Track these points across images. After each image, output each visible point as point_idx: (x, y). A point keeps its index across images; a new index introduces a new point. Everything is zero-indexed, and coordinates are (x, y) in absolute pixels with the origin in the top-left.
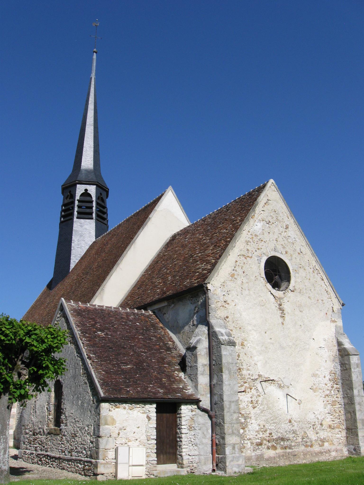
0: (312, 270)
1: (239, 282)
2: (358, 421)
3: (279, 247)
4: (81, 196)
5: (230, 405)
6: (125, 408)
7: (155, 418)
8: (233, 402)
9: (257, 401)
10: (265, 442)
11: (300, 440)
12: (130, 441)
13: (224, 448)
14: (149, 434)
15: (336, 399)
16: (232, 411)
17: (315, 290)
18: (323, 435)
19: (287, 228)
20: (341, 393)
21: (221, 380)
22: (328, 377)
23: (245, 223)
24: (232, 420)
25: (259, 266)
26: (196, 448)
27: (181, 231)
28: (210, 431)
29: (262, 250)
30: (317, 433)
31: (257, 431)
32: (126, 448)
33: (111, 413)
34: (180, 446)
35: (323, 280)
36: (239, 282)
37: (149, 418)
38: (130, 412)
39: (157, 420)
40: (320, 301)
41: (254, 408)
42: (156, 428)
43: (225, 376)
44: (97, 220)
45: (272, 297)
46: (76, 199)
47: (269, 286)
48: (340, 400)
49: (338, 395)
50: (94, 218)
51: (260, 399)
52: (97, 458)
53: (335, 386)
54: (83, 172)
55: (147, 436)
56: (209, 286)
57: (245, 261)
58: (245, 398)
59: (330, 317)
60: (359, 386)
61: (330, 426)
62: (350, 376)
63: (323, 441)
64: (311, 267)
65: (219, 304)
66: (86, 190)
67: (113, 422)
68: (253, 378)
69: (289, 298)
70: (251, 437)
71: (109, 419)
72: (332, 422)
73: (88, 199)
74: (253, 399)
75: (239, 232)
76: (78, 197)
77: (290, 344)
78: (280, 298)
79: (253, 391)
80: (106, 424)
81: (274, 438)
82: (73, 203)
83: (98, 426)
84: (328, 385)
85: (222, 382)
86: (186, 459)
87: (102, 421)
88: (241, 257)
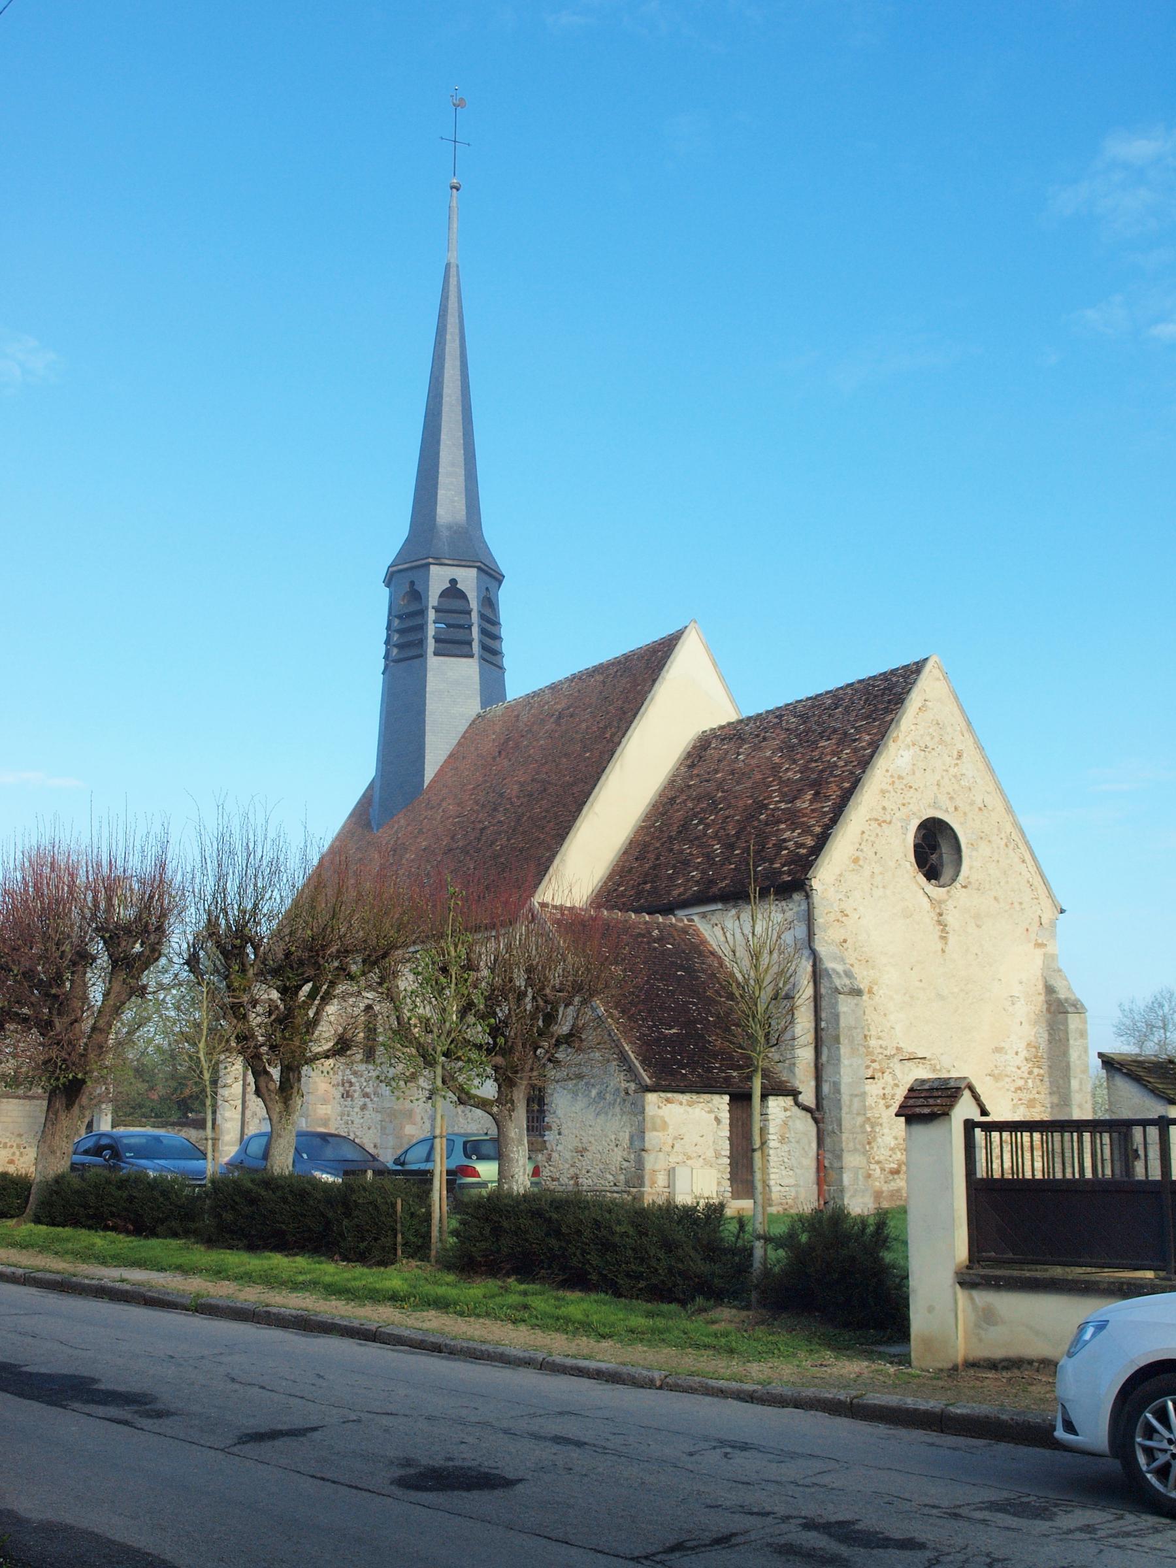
0: (1003, 843)
1: (866, 872)
3: (944, 800)
4: (441, 596)
5: (851, 1101)
6: (681, 1104)
8: (856, 1096)
9: (893, 1095)
12: (689, 1158)
13: (841, 1174)
15: (1037, 1096)
17: (1007, 882)
19: (960, 756)
21: (836, 1060)
22: (1024, 1054)
23: (880, 754)
25: (904, 840)
27: (722, 728)
28: (814, 1145)
29: (911, 806)
31: (892, 1149)
32: (687, 1171)
33: (660, 1112)
35: (1023, 861)
36: (866, 872)
39: (731, 1125)
40: (1016, 905)
42: (730, 1139)
43: (844, 1050)
45: (926, 899)
46: (430, 606)
47: (921, 879)
50: (476, 656)
52: (642, 1185)
53: (1036, 1071)
54: (445, 533)
55: (715, 1151)
56: (815, 884)
57: (878, 830)
59: (1033, 936)
62: (1065, 1053)
64: (1003, 835)
66: (453, 582)
67: (665, 1125)
68: (888, 1053)
69: (957, 899)
70: (882, 1158)
71: (659, 1121)
73: (457, 604)
74: (886, 1092)
75: (868, 771)
76: (433, 600)
77: (956, 990)
78: (940, 902)
79: (887, 1077)
82: (422, 613)
84: (1023, 1069)
85: (839, 1060)
86: (776, 1192)
87: (648, 1125)
88: (872, 823)
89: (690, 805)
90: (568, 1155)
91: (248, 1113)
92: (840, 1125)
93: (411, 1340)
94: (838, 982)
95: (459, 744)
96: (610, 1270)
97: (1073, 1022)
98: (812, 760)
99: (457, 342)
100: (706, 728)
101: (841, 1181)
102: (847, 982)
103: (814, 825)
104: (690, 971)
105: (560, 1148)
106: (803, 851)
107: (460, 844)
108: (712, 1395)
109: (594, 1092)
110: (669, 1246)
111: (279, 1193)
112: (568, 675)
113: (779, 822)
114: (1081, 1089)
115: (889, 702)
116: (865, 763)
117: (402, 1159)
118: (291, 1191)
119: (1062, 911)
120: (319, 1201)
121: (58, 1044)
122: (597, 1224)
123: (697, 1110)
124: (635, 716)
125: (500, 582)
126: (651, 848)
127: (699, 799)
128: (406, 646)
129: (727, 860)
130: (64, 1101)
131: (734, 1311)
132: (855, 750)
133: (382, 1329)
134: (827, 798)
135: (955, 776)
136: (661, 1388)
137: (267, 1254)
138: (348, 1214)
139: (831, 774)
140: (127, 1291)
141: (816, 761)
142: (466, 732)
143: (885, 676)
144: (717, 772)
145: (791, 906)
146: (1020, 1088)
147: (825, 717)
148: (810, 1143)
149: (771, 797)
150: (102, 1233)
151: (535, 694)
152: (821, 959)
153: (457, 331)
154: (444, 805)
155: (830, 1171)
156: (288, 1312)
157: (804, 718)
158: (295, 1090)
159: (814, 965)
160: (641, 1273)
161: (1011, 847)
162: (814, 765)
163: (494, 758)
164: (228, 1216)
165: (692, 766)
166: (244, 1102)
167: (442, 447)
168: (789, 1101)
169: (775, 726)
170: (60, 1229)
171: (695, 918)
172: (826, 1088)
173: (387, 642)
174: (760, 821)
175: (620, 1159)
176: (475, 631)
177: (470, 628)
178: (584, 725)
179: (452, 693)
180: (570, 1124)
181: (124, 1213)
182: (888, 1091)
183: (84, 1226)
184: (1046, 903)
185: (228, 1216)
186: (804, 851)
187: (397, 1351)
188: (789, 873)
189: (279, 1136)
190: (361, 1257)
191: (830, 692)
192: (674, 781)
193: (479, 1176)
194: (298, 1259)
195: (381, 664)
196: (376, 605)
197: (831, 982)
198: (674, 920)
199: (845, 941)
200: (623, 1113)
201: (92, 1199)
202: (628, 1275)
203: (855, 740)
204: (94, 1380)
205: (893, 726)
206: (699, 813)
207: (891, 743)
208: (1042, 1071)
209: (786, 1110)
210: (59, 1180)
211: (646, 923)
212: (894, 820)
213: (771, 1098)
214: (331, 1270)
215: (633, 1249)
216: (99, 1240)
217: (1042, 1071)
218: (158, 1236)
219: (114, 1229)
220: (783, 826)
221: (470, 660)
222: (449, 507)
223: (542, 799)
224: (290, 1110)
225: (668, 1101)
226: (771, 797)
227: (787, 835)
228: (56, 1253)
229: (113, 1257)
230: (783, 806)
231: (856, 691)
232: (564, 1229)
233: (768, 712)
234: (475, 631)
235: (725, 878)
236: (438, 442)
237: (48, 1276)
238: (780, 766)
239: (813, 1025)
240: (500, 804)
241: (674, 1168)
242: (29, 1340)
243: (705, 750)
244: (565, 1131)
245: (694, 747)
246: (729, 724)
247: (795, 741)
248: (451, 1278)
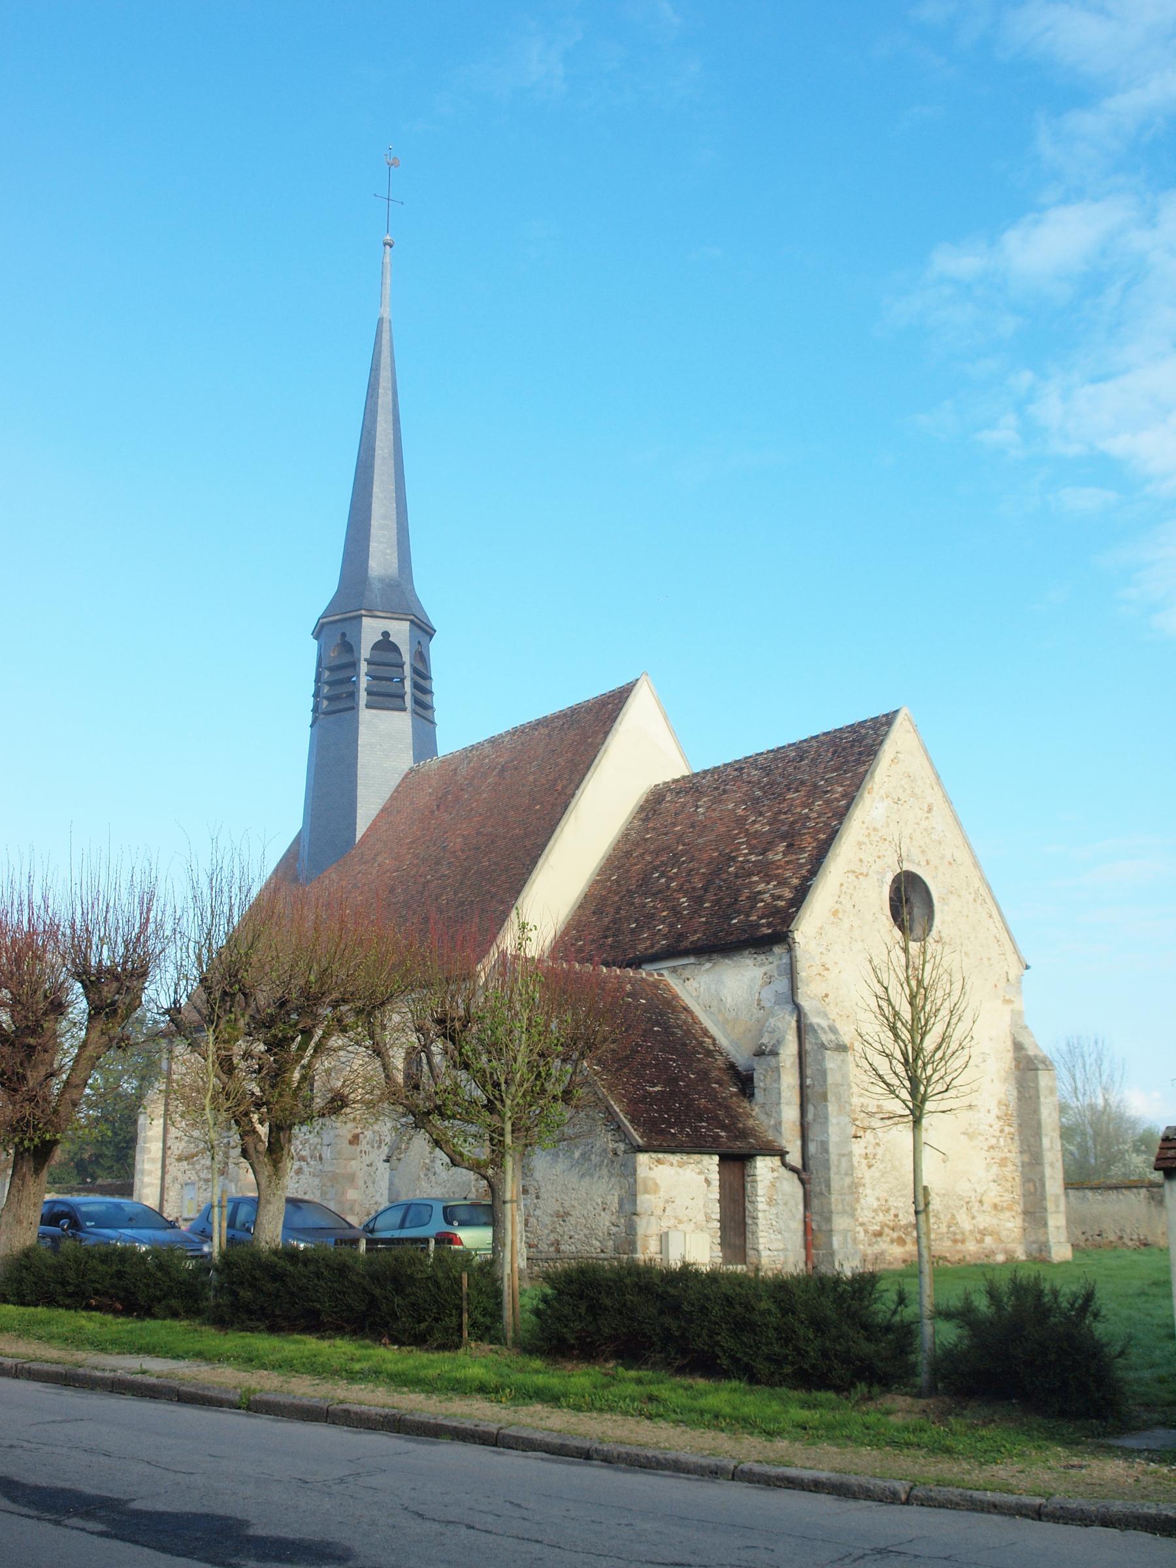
2: (1048, 1197)
6: (672, 1165)
7: (718, 1183)
8: (844, 1155)
9: (875, 1155)
10: (887, 1230)
11: (944, 1229)
12: (680, 1222)
14: (709, 1211)
15: (1008, 1155)
16: (843, 1172)
17: (976, 938)
18: (984, 1221)
19: (930, 810)
20: (1017, 1143)
22: (995, 1111)
23: (857, 805)
24: (842, 1188)
26: (779, 1236)
27: (676, 781)
28: (801, 1207)
30: (973, 1218)
31: (875, 1211)
34: (753, 1233)
37: (708, 1181)
38: (679, 1169)
40: (985, 961)
41: (870, 1167)
42: (719, 1201)
43: (832, 1108)
44: (415, 712)
48: (1014, 1156)
49: (1011, 1147)
51: (880, 1151)
52: (634, 1251)
53: (1007, 1129)
54: (377, 585)
55: (706, 1214)
56: (798, 936)
58: (857, 1148)
60: (1054, 1130)
61: (995, 1206)
63: (983, 1233)
65: (814, 971)
66: (386, 634)
70: (865, 1220)
71: (650, 1183)
72: (999, 1199)
73: (390, 657)
76: (365, 652)
80: (646, 1192)
81: (902, 1223)
82: (354, 665)
83: (632, 1196)
84: (995, 1127)
85: (826, 1118)
87: (640, 1187)
88: (850, 875)
89: (648, 858)
90: (547, 1220)
91: (168, 1178)
92: (828, 1186)
93: (548, 1444)
94: (825, 1038)
95: (392, 798)
96: (745, 1353)
97: (1044, 1080)
98: (780, 812)
99: (390, 397)
100: (659, 781)
101: (831, 1245)
102: (833, 1038)
103: (791, 877)
104: (667, 1028)
105: (538, 1212)
106: (782, 903)
107: (401, 898)
108: (982, 1511)
109: (577, 1154)
110: (819, 1325)
111: (312, 1268)
112: (509, 728)
113: (750, 875)
114: (1052, 1148)
115: (860, 753)
116: (842, 815)
117: (371, 1226)
118: (327, 1266)
119: (1027, 967)
120: (363, 1277)
121: (30, 1100)
122: (729, 1301)
123: (688, 1171)
124: (588, 768)
125: (431, 636)
126: (609, 902)
127: (657, 853)
128: (335, 701)
129: (695, 913)
130: (32, 1164)
131: (909, 1400)
132: (828, 802)
133: (507, 1431)
134: (803, 850)
135: (925, 830)
136: (907, 1502)
137: (297, 1337)
138: (399, 1291)
139: (804, 826)
140: (154, 1386)
141: (785, 813)
142: (399, 786)
143: (852, 729)
144: (674, 825)
145: (770, 959)
146: (992, 1147)
147: (791, 770)
148: (797, 1205)
149: (739, 850)
150: (84, 1313)
151: (473, 748)
152: (805, 1014)
153: (390, 385)
154: (380, 859)
155: (819, 1235)
156: (373, 1410)
157: (767, 770)
158: (285, 1152)
159: (798, 1021)
160: (786, 1357)
161: (979, 901)
162: (783, 817)
163: (432, 812)
164: (246, 1294)
165: (646, 820)
166: (164, 1166)
167: (374, 500)
168: (776, 1161)
169: (735, 779)
170: (32, 1309)
171: (665, 972)
172: (812, 1148)
173: (316, 695)
174: (729, 874)
175: (607, 1224)
176: (408, 684)
177: (403, 682)
178: (531, 778)
179: (384, 746)
180: (549, 1187)
181: (113, 1291)
182: (870, 1150)
183: (60, 1306)
184: (1012, 958)
185: (246, 1294)
186: (783, 903)
187: (527, 1457)
188: (769, 925)
189: (268, 1202)
190: (419, 1340)
191: (794, 744)
192: (627, 835)
193: (461, 1243)
194: (338, 1342)
195: (309, 717)
196: (302, 660)
197: (817, 1038)
198: (644, 975)
199: (827, 996)
200: (611, 1175)
201: (71, 1275)
202: (768, 1358)
203: (828, 792)
204: (245, 1524)
205: (868, 777)
206: (659, 866)
207: (866, 795)
208: (1012, 1130)
209: (773, 1170)
210: (27, 1254)
211: (617, 977)
212: (871, 873)
213: (759, 1158)
214: (387, 1355)
215: (776, 1329)
216: (89, 1322)
217: (1012, 1130)
218: (154, 1316)
219: (97, 1308)
220: (755, 878)
221: (403, 713)
222: (381, 560)
223: (491, 852)
224: (280, 1174)
225: (659, 1161)
226: (739, 850)
227: (761, 887)
228: (40, 1338)
229: (114, 1342)
230: (753, 858)
231: (823, 744)
232: (686, 1307)
233: (725, 765)
234: (408, 684)
235: (696, 932)
236: (371, 496)
237: (46, 1367)
238: (745, 818)
239: (798, 1082)
240: (443, 858)
241: (667, 1234)
242: (102, 1459)
243: (660, 803)
244: (543, 1195)
245: (647, 801)
246: (684, 777)
247: (759, 793)
248: (537, 1364)
